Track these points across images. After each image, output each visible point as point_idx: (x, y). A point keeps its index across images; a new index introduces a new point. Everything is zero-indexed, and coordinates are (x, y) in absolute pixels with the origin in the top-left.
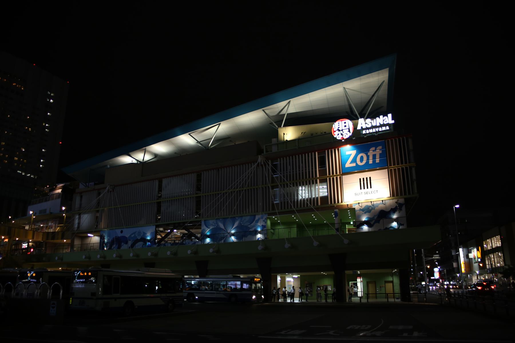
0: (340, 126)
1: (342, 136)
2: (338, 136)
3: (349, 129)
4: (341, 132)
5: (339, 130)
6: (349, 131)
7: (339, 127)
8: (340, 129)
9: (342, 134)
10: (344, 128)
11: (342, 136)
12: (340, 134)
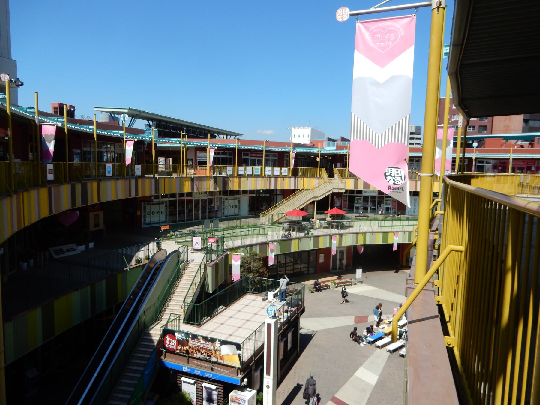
1: (394, 182)
2: (390, 181)
3: (401, 177)
4: (394, 178)
5: (392, 176)
6: (347, 16)
7: (391, 173)
8: (393, 175)
9: (394, 180)
10: (396, 175)
11: (394, 182)
12: (392, 180)
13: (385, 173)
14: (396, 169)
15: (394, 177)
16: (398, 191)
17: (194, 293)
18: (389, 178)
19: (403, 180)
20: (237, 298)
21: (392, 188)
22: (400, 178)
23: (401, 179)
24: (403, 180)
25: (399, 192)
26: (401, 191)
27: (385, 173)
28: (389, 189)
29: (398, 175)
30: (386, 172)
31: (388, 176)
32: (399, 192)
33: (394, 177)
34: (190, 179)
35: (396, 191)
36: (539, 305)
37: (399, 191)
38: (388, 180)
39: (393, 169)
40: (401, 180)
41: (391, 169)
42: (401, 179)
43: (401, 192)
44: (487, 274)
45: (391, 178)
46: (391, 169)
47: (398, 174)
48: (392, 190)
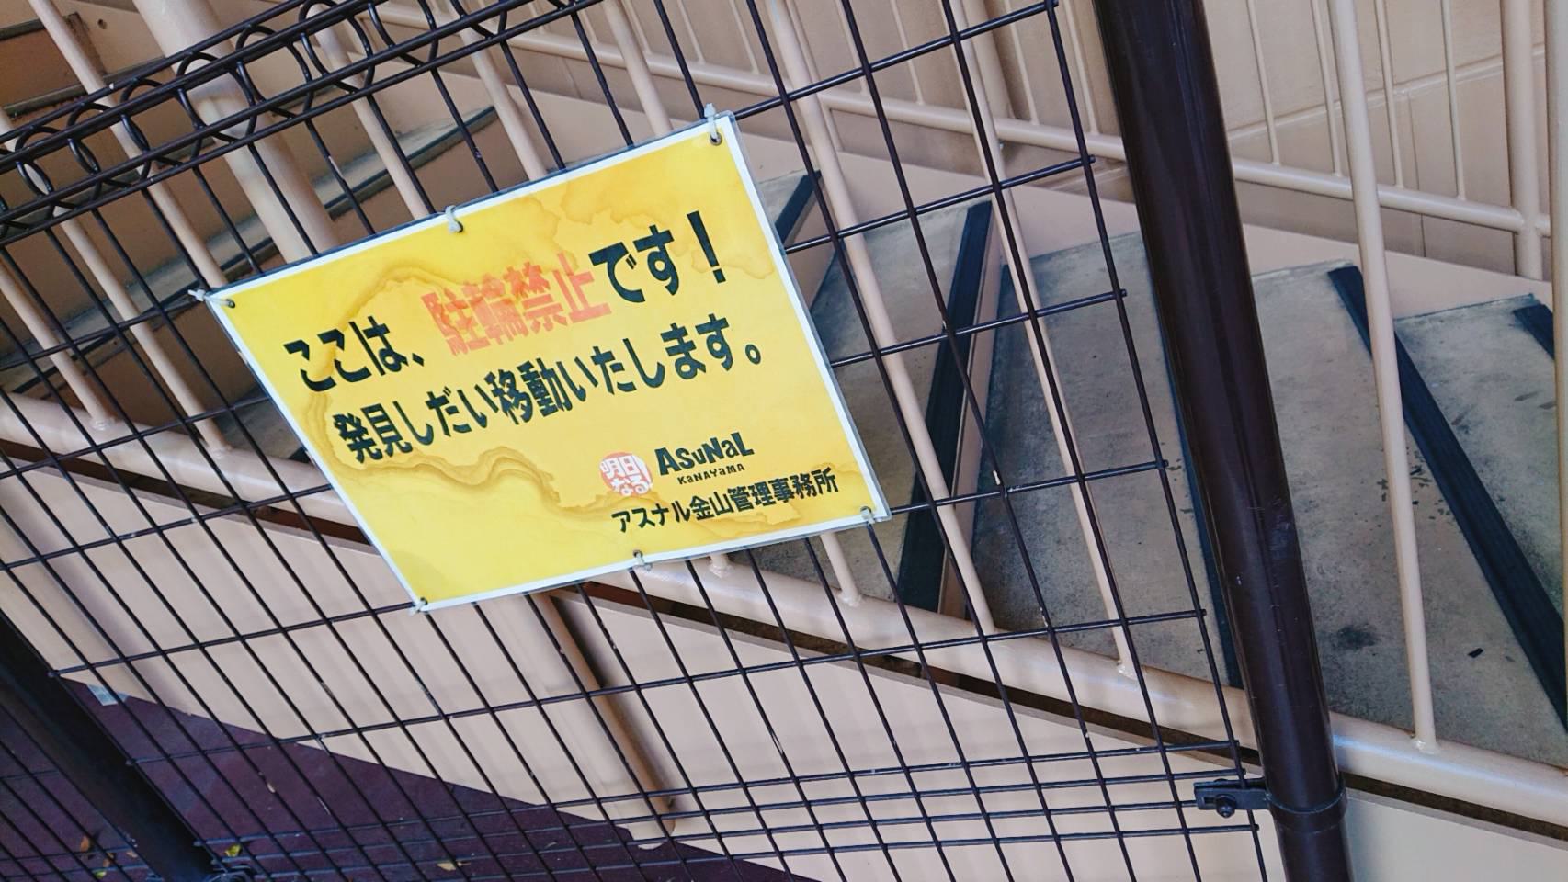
0: (619, 468)
2: (623, 490)
3: (642, 474)
5: (621, 478)
8: (622, 474)
9: (630, 486)
10: (629, 473)
13: (604, 476)
14: (622, 459)
15: (627, 477)
16: (721, 463)
17: (913, 656)
18: (617, 483)
19: (649, 480)
20: (1556, 536)
21: (678, 460)
22: (640, 477)
23: (644, 479)
24: (649, 480)
25: (731, 469)
26: (739, 459)
27: (604, 476)
28: (664, 471)
29: (632, 473)
30: (604, 471)
31: (612, 480)
32: (731, 469)
33: (627, 477)
34: (746, 556)
35: (708, 467)
36: (1565, 684)
37: (727, 461)
38: (617, 490)
39: (615, 460)
40: (644, 483)
41: (612, 462)
42: (644, 479)
43: (741, 467)
44: (1229, 609)
45: (622, 482)
46: (612, 462)
47: (631, 469)
48: (684, 472)
